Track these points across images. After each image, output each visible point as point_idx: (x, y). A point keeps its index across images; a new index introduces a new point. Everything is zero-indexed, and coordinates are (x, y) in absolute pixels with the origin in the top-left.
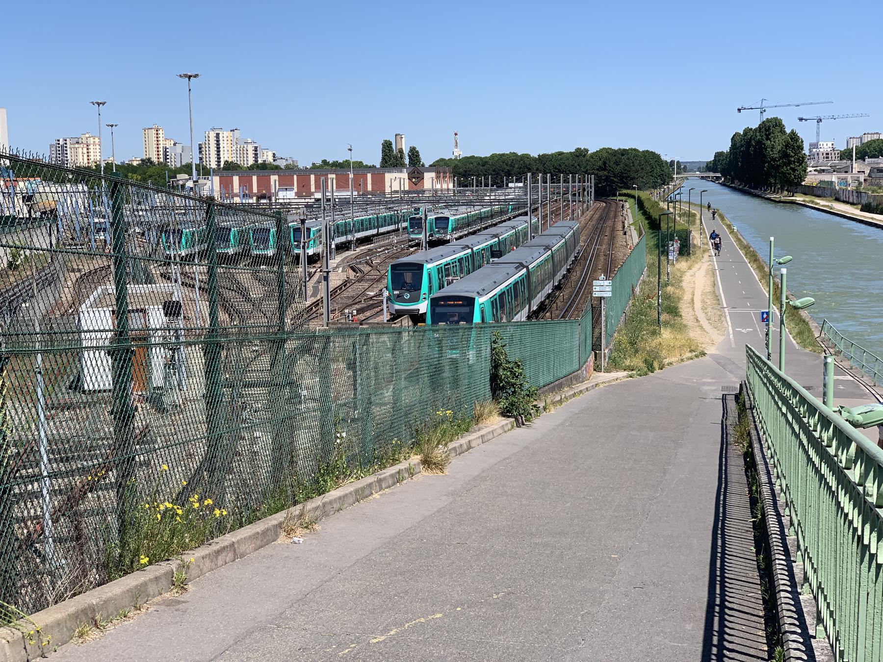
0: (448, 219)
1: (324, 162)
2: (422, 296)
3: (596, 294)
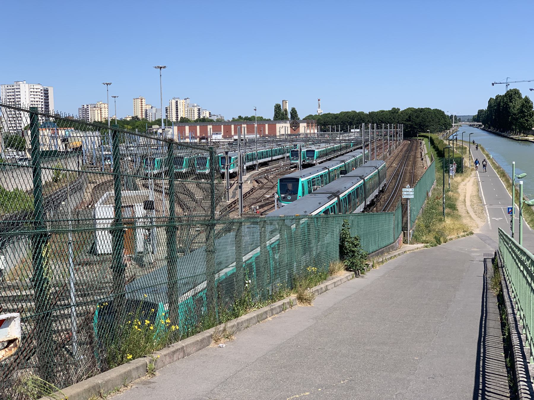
0: (314, 151)
1: (240, 117)
3: (404, 197)
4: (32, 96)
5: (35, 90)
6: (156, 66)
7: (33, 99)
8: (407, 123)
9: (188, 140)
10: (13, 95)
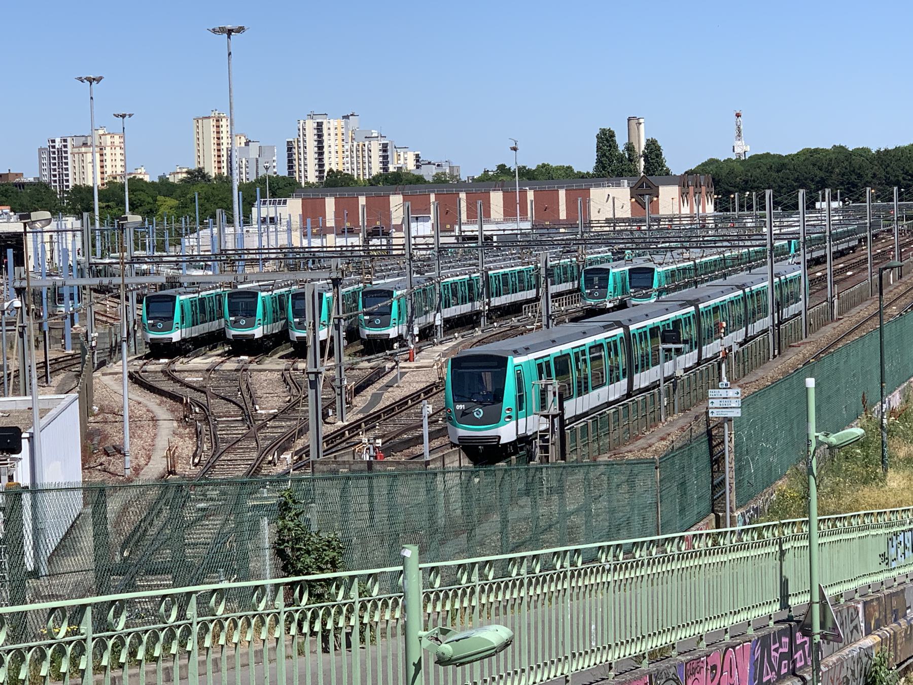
1: (502, 168)
6: (217, 27)
9: (331, 240)
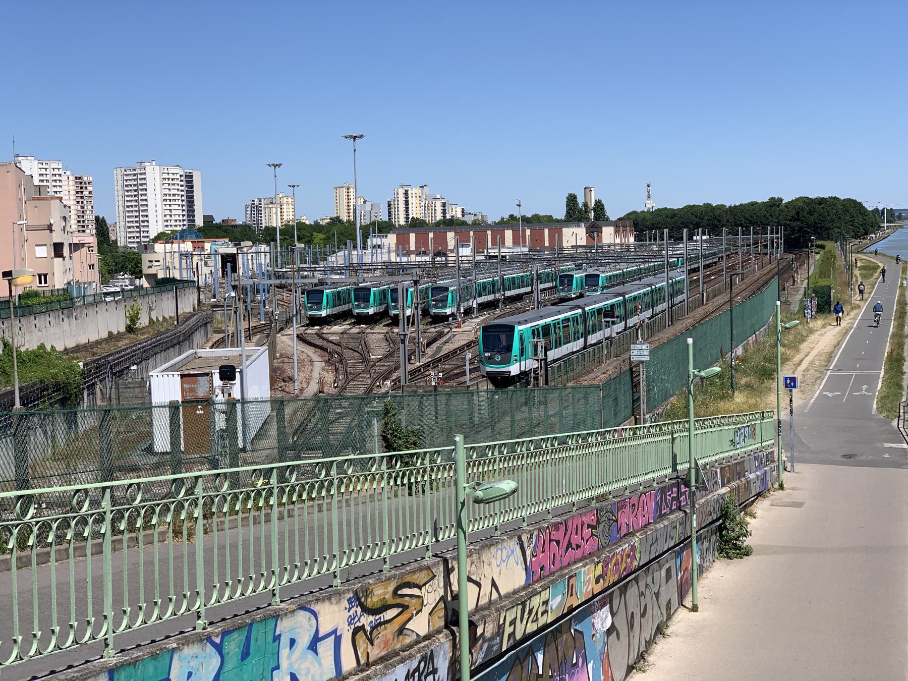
2: (513, 358)
3: (635, 359)
4: (166, 186)
5: (171, 176)
7: (167, 192)
8: (794, 224)
9: (413, 258)
10: (135, 185)
